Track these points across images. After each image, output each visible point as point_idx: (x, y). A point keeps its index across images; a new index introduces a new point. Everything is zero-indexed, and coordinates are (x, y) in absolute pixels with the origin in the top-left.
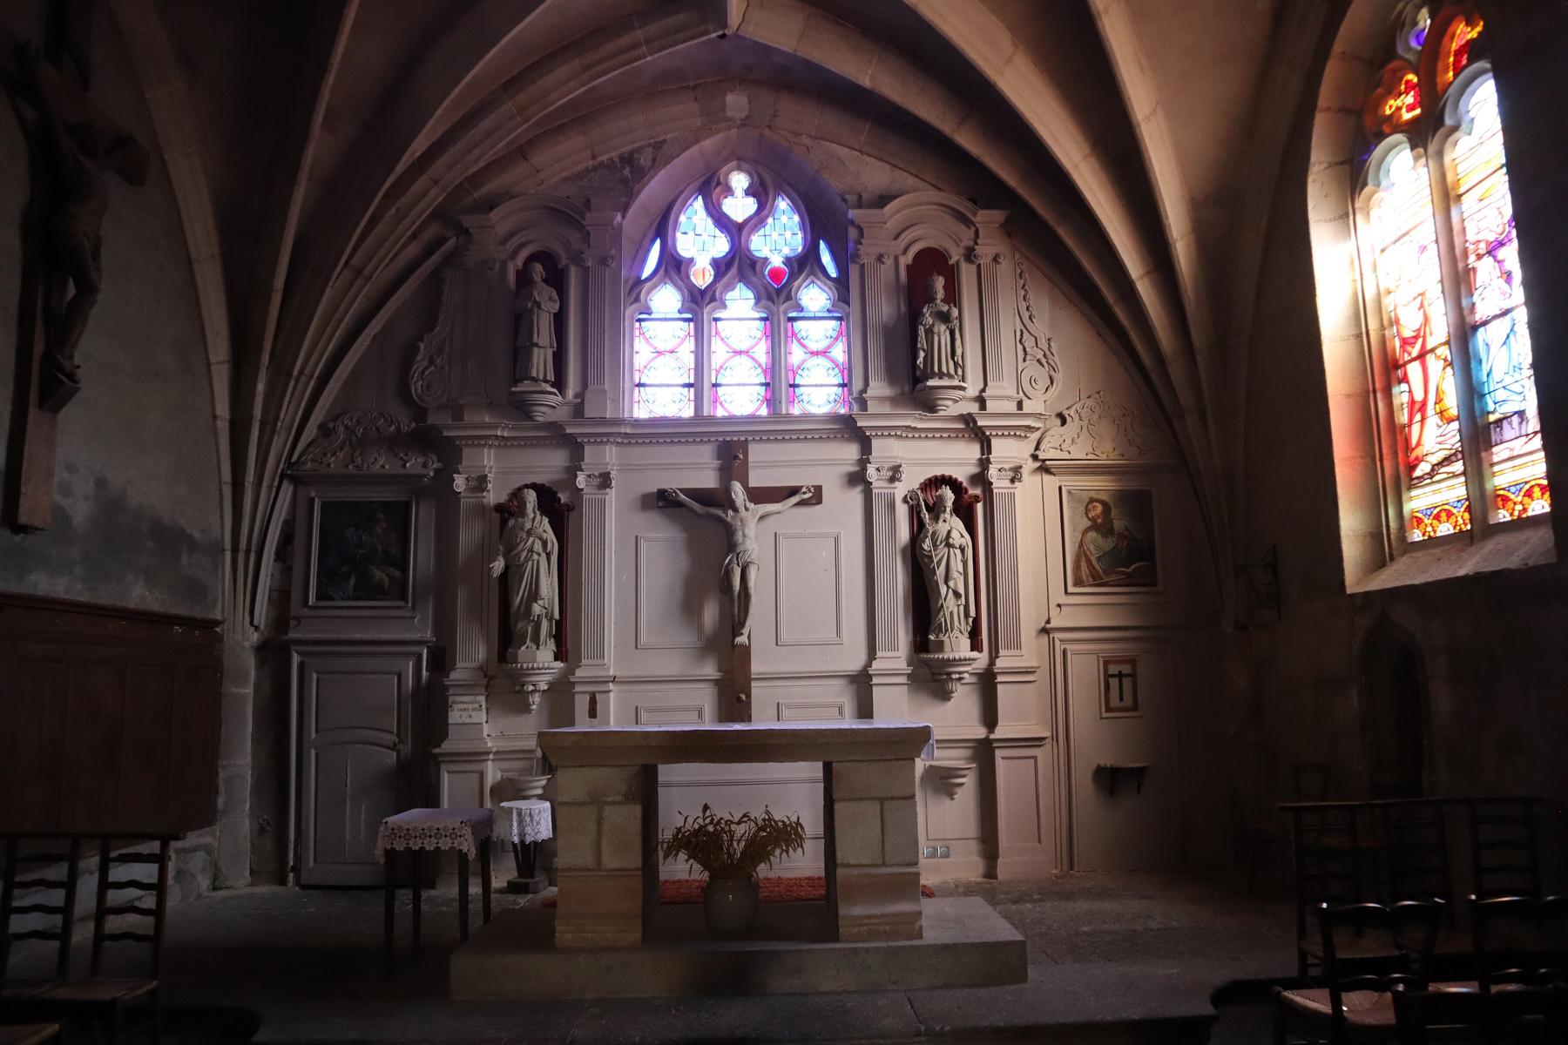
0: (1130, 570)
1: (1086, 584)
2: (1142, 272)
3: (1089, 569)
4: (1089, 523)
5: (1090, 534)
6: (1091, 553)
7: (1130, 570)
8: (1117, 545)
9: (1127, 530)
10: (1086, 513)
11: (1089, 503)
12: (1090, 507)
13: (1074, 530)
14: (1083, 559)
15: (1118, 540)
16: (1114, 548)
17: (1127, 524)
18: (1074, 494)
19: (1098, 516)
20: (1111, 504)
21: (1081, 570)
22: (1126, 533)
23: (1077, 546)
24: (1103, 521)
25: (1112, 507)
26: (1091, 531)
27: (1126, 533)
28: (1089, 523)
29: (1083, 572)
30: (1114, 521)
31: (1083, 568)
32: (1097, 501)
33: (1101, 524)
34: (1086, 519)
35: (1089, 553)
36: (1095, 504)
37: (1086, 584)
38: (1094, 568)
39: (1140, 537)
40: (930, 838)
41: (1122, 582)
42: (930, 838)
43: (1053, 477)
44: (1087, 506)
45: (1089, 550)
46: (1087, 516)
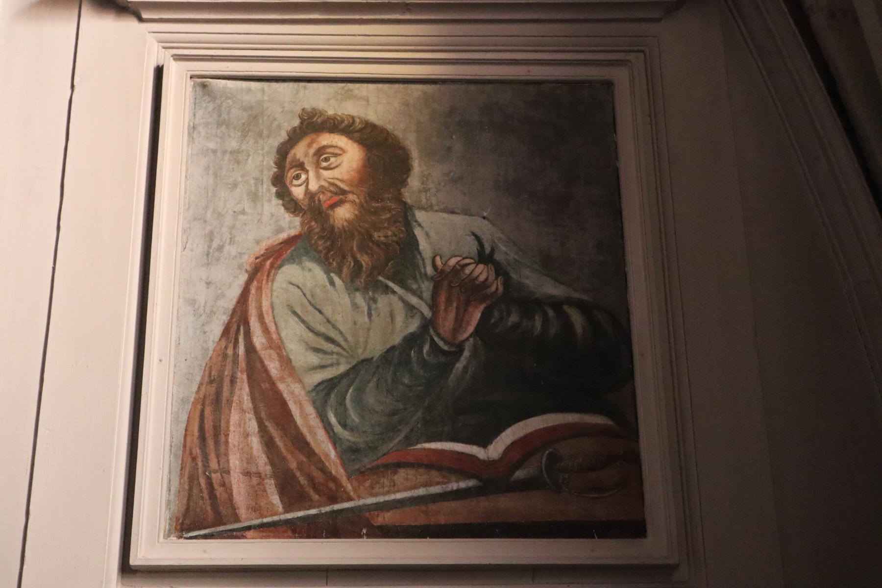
0: (496, 449)
1: (247, 518)
2: (243, 354)
3: (269, 444)
4: (291, 225)
5: (289, 273)
6: (286, 362)
7: (496, 449)
8: (427, 325)
9: (484, 257)
10: (279, 180)
11: (295, 137)
12: (300, 151)
13: (211, 256)
14: (243, 392)
15: (433, 305)
16: (412, 341)
17: (486, 230)
18: (229, 95)
19: (340, 195)
20: (411, 142)
21: (222, 455)
22: (482, 272)
23: (216, 329)
24: (364, 210)
25: (415, 153)
26: (292, 260)
27: (482, 272)
28: (291, 225)
29: (235, 462)
30: (420, 215)
31: (234, 439)
32: (334, 125)
33: (349, 232)
34: (273, 207)
35: (273, 367)
36: (326, 139)
37: (247, 518)
38: (300, 443)
39: (551, 289)
40: (137, 558)
41: (444, 513)
42: (137, 558)
43: (130, 25)
44: (283, 152)
45: (278, 347)
46: (283, 194)
